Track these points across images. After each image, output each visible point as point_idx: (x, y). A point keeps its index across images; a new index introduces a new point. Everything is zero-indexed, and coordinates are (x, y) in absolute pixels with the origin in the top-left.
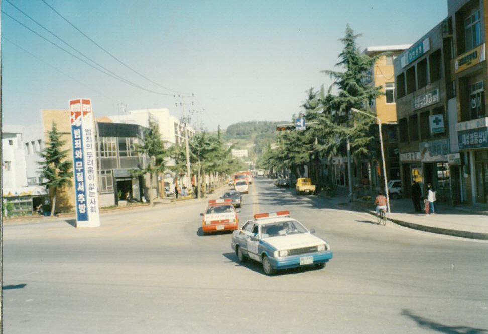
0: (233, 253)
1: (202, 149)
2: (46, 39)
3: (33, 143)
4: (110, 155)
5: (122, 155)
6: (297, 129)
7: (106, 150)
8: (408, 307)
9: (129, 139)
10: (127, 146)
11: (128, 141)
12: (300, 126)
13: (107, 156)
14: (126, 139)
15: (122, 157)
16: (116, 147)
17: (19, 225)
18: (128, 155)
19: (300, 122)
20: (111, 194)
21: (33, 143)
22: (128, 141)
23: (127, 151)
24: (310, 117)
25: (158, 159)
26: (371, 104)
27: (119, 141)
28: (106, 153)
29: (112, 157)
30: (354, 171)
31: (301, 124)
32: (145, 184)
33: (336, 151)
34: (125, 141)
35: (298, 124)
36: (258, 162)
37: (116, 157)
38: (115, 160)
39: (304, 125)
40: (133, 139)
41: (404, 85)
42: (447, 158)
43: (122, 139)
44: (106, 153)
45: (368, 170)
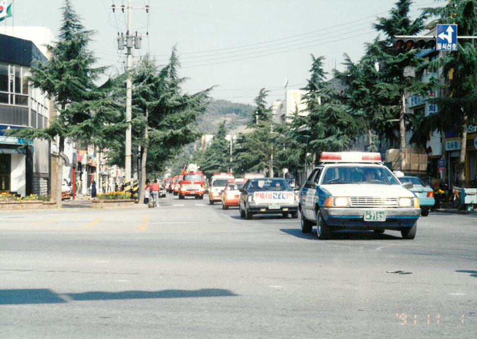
0: (299, 230)
1: (155, 103)
8: (313, 54)
9: (14, 68)
10: (9, 82)
11: (12, 72)
12: (445, 41)
14: (9, 67)
17: (12, 203)
19: (447, 33)
21: (279, 198)
22: (12, 72)
23: (9, 92)
24: (453, 64)
25: (308, 183)
31: (449, 38)
34: (7, 72)
35: (442, 36)
36: (164, 85)
40: (22, 69)
42: (314, 198)
45: (2, 186)
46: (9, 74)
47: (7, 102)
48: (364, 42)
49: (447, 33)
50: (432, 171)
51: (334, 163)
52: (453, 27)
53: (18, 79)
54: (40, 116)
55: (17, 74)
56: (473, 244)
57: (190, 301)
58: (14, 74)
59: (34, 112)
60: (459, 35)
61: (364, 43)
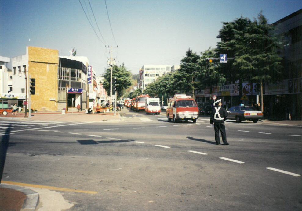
2: (108, 13)
3: (19, 67)
4: (66, 79)
5: (72, 79)
6: (221, 62)
7: (63, 75)
11: (76, 71)
12: (223, 60)
13: (63, 79)
14: (75, 70)
15: (72, 81)
16: (69, 74)
18: (75, 79)
19: (223, 57)
20: (63, 104)
21: (19, 67)
22: (76, 71)
26: (192, 56)
27: (71, 70)
28: (63, 77)
29: (67, 80)
30: (180, 146)
31: (224, 58)
32: (67, 104)
33: (225, 79)
37: (69, 80)
38: (68, 82)
39: (226, 60)
41: (266, 132)
43: (73, 69)
44: (63, 77)
46: (75, 72)
47: (74, 80)
48: (180, 61)
49: (223, 57)
50: (245, 107)
51: (253, 113)
52: (226, 55)
53: (78, 73)
54: (84, 84)
55: (78, 72)
56: (300, 147)
57: (39, 91)
58: (76, 72)
59: (82, 83)
60: (228, 57)
61: (180, 61)
